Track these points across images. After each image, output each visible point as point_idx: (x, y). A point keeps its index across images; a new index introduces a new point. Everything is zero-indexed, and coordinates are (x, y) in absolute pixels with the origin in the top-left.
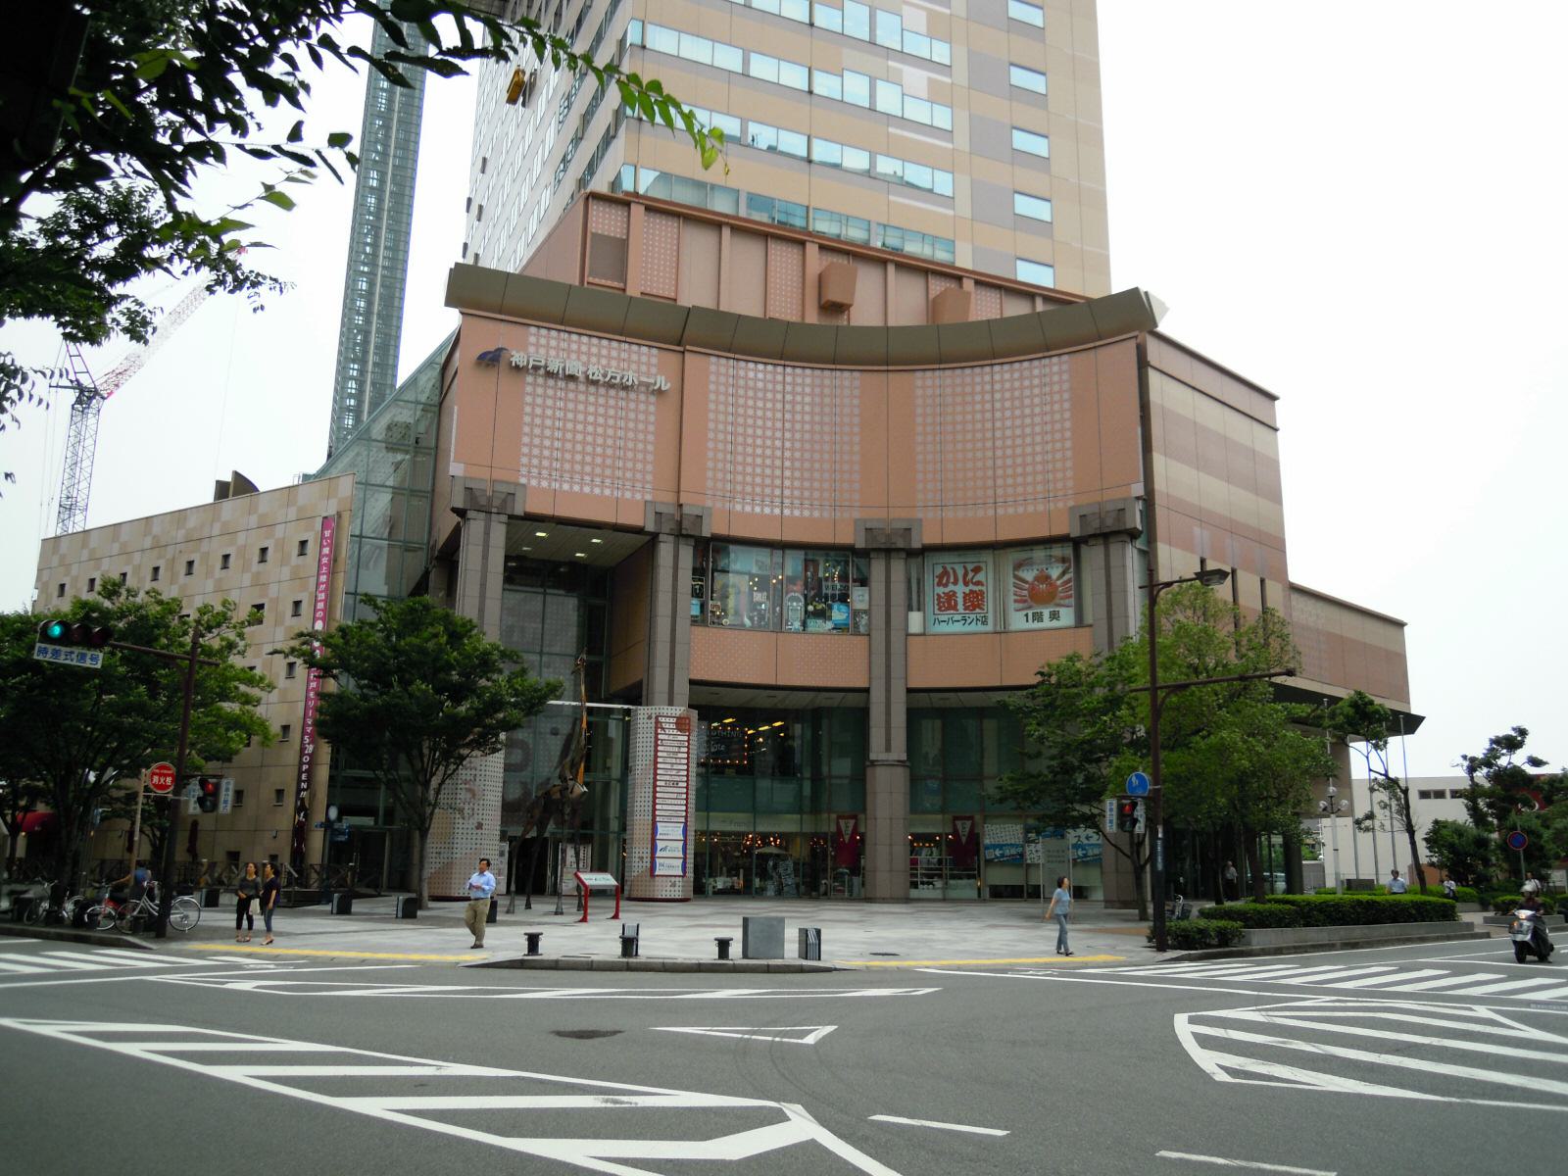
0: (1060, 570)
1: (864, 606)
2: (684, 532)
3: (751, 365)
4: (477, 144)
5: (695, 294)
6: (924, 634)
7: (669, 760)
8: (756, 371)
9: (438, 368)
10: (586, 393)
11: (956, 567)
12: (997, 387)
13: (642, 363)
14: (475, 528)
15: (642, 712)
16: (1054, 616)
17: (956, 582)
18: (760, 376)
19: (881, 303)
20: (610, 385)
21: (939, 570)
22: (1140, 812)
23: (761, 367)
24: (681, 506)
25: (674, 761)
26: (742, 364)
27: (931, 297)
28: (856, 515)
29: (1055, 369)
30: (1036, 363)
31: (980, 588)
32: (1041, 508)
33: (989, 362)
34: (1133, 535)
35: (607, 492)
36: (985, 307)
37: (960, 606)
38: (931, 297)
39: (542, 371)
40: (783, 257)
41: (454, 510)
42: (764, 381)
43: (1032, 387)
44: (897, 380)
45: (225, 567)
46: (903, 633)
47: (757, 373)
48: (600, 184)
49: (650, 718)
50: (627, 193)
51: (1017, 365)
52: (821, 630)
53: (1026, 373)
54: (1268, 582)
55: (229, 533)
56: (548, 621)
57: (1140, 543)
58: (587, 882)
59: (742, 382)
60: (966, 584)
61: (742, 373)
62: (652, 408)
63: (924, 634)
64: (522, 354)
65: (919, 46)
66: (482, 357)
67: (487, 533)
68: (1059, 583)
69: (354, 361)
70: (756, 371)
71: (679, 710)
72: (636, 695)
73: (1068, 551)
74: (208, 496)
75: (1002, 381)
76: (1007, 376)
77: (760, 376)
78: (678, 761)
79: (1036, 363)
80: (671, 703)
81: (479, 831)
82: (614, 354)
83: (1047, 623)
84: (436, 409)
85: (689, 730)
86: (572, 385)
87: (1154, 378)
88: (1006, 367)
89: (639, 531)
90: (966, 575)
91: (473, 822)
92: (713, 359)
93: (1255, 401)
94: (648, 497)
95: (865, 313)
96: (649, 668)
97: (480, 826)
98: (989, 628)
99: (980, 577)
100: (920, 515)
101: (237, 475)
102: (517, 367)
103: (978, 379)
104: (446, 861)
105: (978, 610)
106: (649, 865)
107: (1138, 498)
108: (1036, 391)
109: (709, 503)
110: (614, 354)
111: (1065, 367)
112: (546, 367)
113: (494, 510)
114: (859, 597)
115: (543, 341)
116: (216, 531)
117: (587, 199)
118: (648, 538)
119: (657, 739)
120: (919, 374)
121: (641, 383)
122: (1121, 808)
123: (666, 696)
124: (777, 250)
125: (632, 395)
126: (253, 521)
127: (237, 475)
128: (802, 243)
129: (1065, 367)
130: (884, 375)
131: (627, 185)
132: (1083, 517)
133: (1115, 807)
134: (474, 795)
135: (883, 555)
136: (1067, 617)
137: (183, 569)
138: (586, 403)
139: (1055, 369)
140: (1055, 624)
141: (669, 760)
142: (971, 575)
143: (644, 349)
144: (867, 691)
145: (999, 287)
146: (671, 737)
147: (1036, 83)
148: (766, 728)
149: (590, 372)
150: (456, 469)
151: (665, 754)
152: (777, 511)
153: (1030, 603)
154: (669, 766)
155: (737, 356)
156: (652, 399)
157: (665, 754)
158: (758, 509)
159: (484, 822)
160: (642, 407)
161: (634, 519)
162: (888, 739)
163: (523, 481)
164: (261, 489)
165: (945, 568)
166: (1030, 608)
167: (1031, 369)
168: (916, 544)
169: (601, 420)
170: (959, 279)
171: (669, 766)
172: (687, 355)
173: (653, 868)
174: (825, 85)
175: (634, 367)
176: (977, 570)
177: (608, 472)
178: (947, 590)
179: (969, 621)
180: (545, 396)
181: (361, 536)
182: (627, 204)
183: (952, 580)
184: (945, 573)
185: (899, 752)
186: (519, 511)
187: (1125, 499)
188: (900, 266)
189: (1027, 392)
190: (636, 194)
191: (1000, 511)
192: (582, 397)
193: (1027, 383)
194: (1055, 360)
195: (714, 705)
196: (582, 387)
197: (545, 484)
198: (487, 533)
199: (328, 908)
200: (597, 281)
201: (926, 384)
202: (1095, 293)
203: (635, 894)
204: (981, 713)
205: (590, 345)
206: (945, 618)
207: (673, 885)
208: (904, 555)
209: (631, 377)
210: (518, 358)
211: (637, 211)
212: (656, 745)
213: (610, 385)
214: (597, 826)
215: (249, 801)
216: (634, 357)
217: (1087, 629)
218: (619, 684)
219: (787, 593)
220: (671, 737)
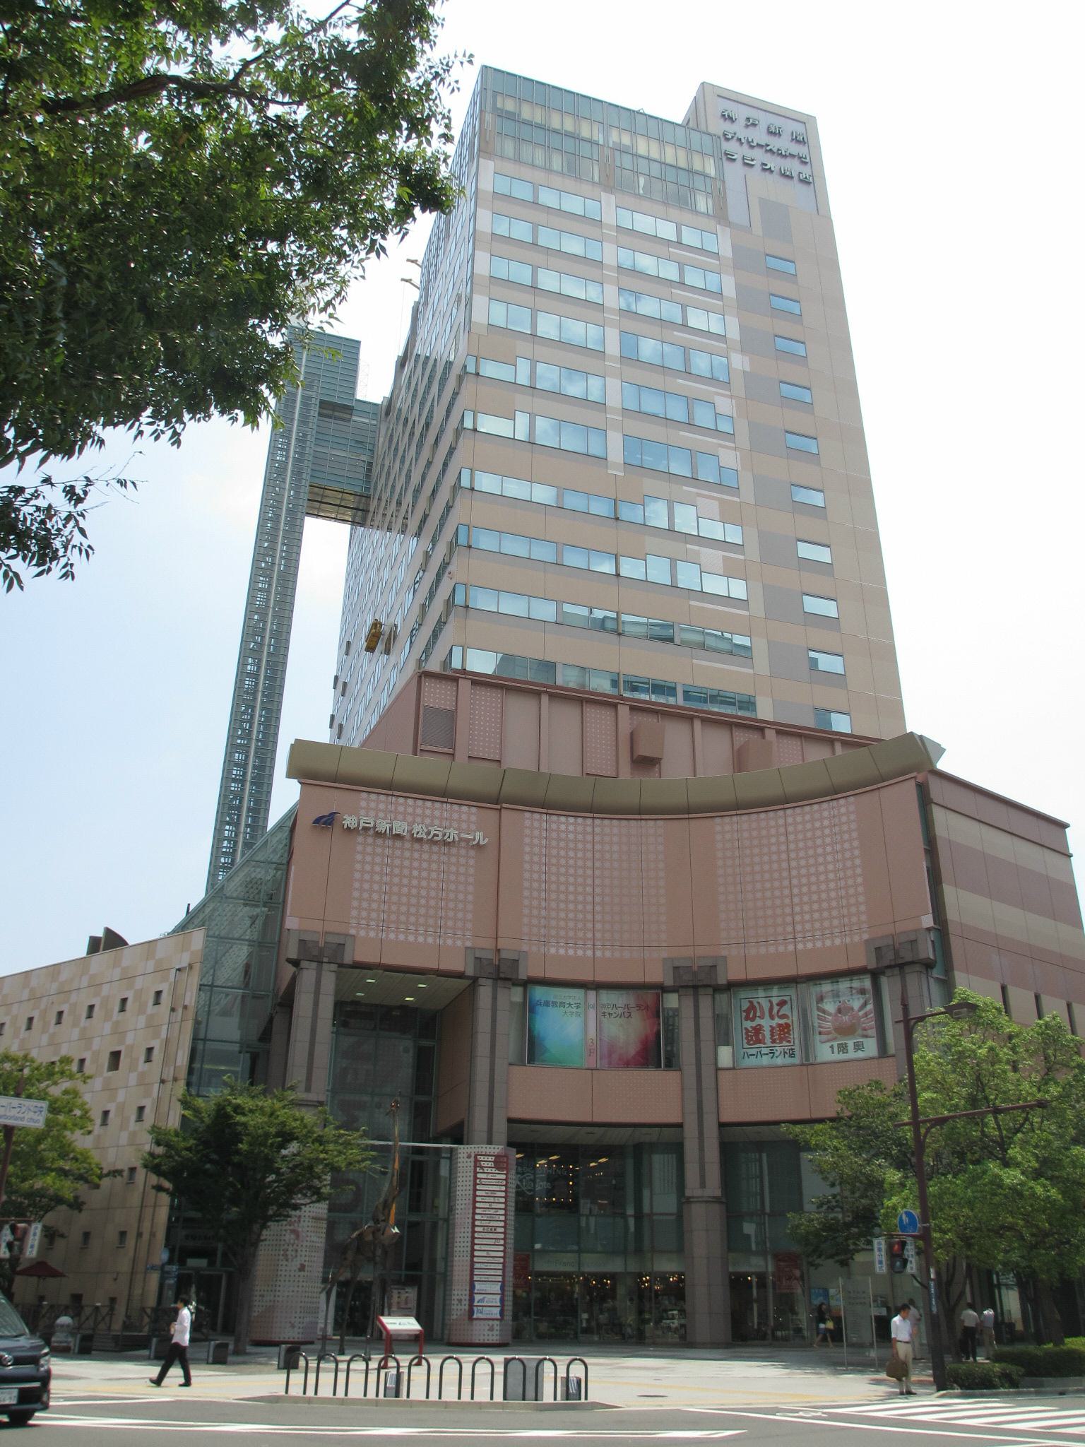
0: (862, 1001)
2: (502, 975)
3: (563, 819)
4: (344, 630)
5: (519, 758)
6: (734, 1068)
7: (487, 1199)
8: (567, 824)
9: (287, 829)
10: (412, 850)
13: (464, 823)
14: (308, 976)
15: (463, 1151)
16: (858, 1047)
18: (571, 828)
19: (693, 759)
20: (432, 842)
21: (745, 1005)
22: (910, 1251)
23: (571, 820)
24: (498, 951)
25: (492, 1200)
26: (555, 818)
27: (736, 747)
28: (664, 954)
29: (843, 810)
30: (825, 805)
32: (838, 942)
34: (928, 965)
35: (430, 940)
37: (768, 1040)
38: (736, 747)
39: (371, 832)
40: (598, 719)
41: (289, 961)
42: (575, 832)
43: (822, 828)
44: (698, 827)
45: (90, 1016)
46: (713, 1067)
47: (567, 826)
48: (434, 665)
49: (469, 1157)
50: (456, 671)
51: (807, 808)
53: (817, 816)
55: (96, 985)
57: (937, 973)
58: (390, 1327)
59: (554, 835)
60: (772, 1018)
61: (554, 826)
62: (472, 862)
63: (734, 1068)
64: (354, 817)
65: (715, 530)
66: (317, 821)
67: (318, 982)
68: (861, 1013)
69: (228, 823)
70: (567, 824)
71: (497, 1149)
72: (458, 1135)
73: (867, 983)
74: (82, 951)
75: (795, 824)
76: (799, 819)
77: (571, 828)
80: (490, 1142)
81: (302, 1273)
82: (437, 813)
83: (852, 1054)
84: (284, 867)
85: (507, 1169)
86: (398, 844)
87: (938, 814)
89: (460, 976)
91: (296, 1264)
92: (527, 815)
93: (1048, 833)
94: (468, 944)
95: (675, 768)
96: (470, 1108)
98: (796, 1060)
99: (785, 1010)
100: (724, 953)
101: (108, 932)
102: (348, 828)
103: (772, 823)
105: (785, 1043)
106: (467, 1307)
107: (929, 929)
108: (827, 831)
109: (525, 948)
110: (437, 813)
112: (375, 827)
113: (325, 960)
115: (373, 805)
116: (85, 983)
117: (420, 677)
118: (467, 982)
119: (476, 1178)
120: (718, 820)
121: (461, 840)
122: (890, 1247)
123: (485, 1135)
124: (592, 713)
125: (454, 851)
126: (117, 973)
127: (108, 932)
128: (615, 706)
129: (852, 808)
130: (876, 793)
131: (456, 664)
132: (878, 949)
133: (883, 1247)
134: (298, 1236)
135: (691, 991)
136: (871, 1047)
137: (53, 1018)
138: (411, 859)
139: (843, 810)
140: (860, 1054)
141: (487, 1199)
143: (465, 809)
144: (680, 1126)
145: (800, 736)
147: (823, 555)
149: (414, 831)
150: (291, 923)
151: (482, 1191)
152: (589, 953)
153: (836, 1035)
154: (487, 1205)
156: (472, 853)
157: (482, 1191)
158: (562, 951)
160: (462, 860)
161: (456, 964)
162: (703, 1172)
163: (352, 932)
164: (130, 943)
166: (835, 1039)
168: (722, 981)
169: (571, 854)
170: (761, 730)
171: (487, 1205)
173: (471, 1312)
174: (631, 568)
175: (455, 824)
176: (782, 1004)
177: (431, 921)
178: (754, 1024)
180: (374, 854)
181: (212, 986)
182: (456, 680)
184: (752, 1007)
185: (714, 1187)
186: (348, 960)
187: (916, 931)
188: (704, 721)
189: (818, 833)
190: (464, 671)
191: (800, 946)
192: (407, 854)
193: (817, 824)
194: (842, 802)
195: (528, 1142)
196: (408, 845)
197: (372, 934)
198: (318, 982)
199: (145, 1352)
200: (428, 748)
201: (724, 828)
202: (887, 736)
203: (454, 1339)
204: (760, 1146)
205: (415, 807)
207: (491, 1329)
208: (710, 991)
209: (452, 834)
210: (350, 821)
211: (465, 685)
212: (475, 1184)
213: (432, 842)
216: (455, 816)
217: (891, 1059)
218: (446, 1123)
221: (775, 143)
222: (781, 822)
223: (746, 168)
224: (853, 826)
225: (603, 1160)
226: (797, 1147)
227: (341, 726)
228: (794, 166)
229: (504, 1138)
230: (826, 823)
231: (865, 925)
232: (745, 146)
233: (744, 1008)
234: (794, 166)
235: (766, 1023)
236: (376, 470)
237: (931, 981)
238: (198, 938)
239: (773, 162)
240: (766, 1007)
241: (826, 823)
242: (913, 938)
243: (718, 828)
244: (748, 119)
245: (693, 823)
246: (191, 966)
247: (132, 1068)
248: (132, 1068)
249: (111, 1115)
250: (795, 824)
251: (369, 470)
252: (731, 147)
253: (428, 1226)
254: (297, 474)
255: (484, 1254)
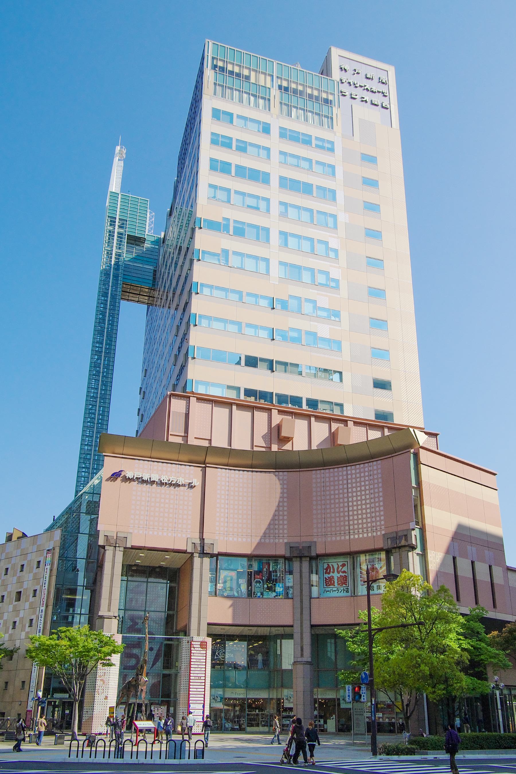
1: (291, 584)
2: (205, 552)
11: (333, 564)
12: (349, 477)
13: (190, 474)
17: (333, 572)
20: (171, 485)
21: (326, 566)
25: (199, 663)
29: (375, 467)
31: (345, 574)
32: (370, 535)
33: (345, 465)
36: (356, 436)
39: (140, 480)
44: (305, 475)
52: (270, 597)
54: (493, 567)
56: (148, 595)
60: (338, 572)
63: (319, 598)
67: (114, 556)
75: (351, 474)
76: (353, 472)
78: (201, 663)
79: (366, 465)
81: (106, 700)
87: (423, 468)
88: (353, 467)
89: (185, 552)
90: (338, 568)
97: (106, 698)
99: (345, 569)
100: (315, 540)
104: (90, 715)
109: (217, 538)
111: (379, 466)
114: (290, 581)
120: (314, 472)
139: (375, 467)
142: (341, 568)
146: (198, 652)
148: (256, 644)
149: (162, 479)
155: (230, 468)
159: (108, 696)
163: (131, 531)
165: (328, 565)
167: (364, 468)
168: (313, 554)
172: (207, 468)
176: (343, 565)
178: (329, 576)
179: (340, 591)
183: (332, 570)
186: (129, 545)
191: (352, 537)
194: (375, 463)
198: (114, 556)
206: (329, 589)
208: (308, 559)
210: (129, 475)
213: (171, 485)
214: (172, 696)
215: (10, 687)
219: (254, 579)
220: (198, 652)
221: (369, 85)
222: (345, 473)
223: (353, 100)
224: (380, 476)
225: (260, 643)
226: (70, 729)
227: (142, 415)
228: (378, 99)
229: (205, 633)
230: (367, 474)
231: (383, 527)
232: (353, 86)
233: (325, 567)
234: (378, 99)
235: (336, 575)
236: (158, 275)
237: (415, 555)
238: (58, 534)
239: (368, 96)
240: (336, 567)
241: (367, 474)
242: (405, 534)
243: (314, 476)
244: (355, 70)
245: (301, 473)
246: (54, 549)
247: (27, 600)
248: (27, 600)
249: (17, 624)
250: (351, 474)
251: (155, 275)
252: (344, 88)
253: (174, 675)
254: (116, 277)
255: (195, 690)
